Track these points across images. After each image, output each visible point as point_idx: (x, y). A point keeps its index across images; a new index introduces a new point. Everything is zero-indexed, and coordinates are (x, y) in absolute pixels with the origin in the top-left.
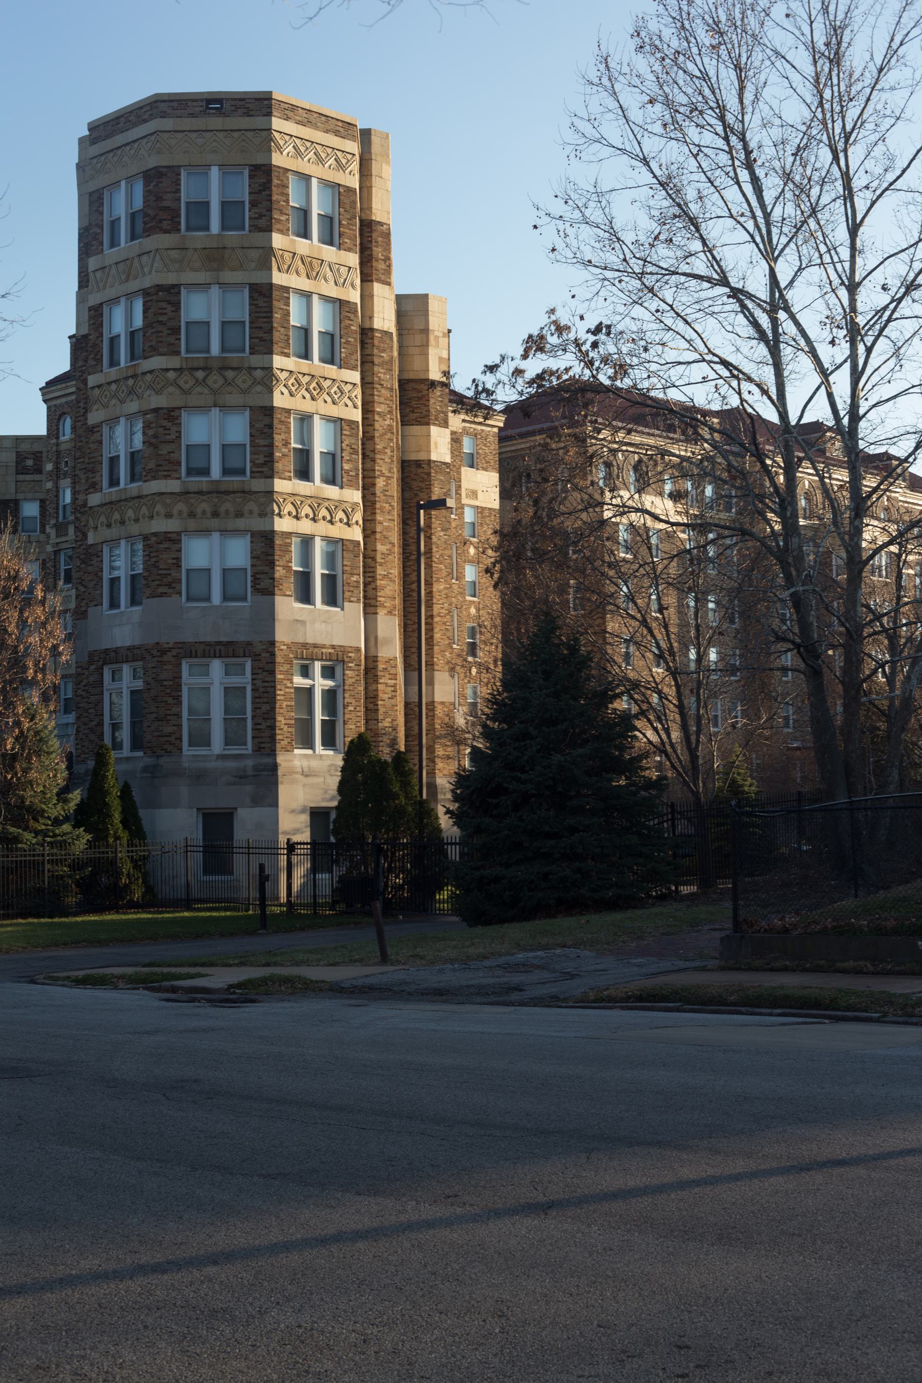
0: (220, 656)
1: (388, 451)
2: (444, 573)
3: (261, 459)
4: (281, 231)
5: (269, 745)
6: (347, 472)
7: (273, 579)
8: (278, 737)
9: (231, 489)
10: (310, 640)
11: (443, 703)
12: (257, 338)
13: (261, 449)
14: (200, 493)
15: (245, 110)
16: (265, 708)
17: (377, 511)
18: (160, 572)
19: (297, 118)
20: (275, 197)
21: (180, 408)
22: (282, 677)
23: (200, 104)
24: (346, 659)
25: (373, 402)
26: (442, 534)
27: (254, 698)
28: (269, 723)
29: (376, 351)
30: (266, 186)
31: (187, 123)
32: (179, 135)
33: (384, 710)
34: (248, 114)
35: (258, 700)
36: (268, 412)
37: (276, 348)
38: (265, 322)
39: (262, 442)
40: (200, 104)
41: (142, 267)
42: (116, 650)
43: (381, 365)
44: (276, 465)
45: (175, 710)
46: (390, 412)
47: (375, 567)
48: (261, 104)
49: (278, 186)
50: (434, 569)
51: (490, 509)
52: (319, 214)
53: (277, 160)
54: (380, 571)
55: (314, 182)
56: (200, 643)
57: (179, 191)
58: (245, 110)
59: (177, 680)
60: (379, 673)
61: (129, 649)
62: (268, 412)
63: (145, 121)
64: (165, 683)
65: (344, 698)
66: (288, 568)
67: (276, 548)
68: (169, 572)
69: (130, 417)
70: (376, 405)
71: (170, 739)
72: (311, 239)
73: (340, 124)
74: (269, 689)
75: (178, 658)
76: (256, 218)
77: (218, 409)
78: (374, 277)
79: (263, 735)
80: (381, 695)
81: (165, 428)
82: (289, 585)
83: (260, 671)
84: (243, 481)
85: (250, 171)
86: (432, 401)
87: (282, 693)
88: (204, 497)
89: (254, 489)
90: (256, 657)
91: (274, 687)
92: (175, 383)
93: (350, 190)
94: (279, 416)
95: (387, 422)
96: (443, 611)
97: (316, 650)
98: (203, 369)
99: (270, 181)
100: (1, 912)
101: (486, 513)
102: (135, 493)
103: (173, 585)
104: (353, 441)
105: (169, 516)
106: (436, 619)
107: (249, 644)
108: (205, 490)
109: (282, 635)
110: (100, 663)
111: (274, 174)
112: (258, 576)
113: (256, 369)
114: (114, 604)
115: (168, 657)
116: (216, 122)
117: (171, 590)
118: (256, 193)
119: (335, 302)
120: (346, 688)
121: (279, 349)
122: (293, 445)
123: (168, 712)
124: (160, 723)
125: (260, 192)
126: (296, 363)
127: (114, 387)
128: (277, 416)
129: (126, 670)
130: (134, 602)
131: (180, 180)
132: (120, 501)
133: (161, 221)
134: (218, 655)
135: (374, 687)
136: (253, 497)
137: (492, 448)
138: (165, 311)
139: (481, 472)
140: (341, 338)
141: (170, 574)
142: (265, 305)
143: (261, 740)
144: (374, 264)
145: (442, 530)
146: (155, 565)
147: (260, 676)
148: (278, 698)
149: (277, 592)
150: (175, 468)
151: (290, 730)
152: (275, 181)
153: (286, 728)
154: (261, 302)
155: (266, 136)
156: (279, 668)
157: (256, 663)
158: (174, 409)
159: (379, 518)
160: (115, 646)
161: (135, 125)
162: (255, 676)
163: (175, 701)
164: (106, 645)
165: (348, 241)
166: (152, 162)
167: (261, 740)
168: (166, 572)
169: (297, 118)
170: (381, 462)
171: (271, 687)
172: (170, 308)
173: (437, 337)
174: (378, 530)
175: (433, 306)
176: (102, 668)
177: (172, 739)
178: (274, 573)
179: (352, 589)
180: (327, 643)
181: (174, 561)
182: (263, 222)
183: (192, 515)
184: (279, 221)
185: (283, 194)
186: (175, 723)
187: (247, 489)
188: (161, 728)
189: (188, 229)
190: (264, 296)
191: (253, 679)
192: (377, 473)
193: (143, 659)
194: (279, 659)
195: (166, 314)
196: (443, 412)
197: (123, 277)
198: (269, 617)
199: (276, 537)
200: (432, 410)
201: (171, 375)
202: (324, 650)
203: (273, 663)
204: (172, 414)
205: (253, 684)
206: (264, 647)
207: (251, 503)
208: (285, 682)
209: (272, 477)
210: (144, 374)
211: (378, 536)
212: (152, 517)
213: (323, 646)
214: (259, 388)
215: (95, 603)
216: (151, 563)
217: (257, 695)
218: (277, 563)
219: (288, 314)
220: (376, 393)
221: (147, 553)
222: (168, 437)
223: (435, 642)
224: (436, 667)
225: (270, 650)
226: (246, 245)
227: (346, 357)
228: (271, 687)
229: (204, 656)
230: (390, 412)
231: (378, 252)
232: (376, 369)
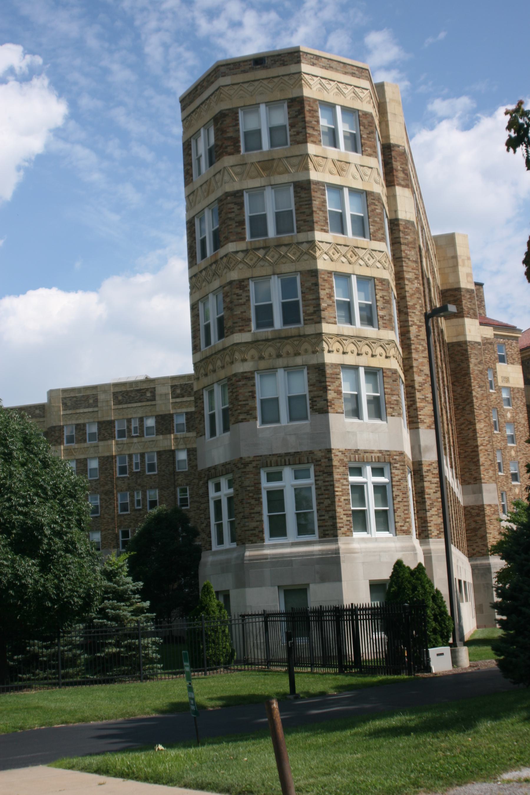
0: (289, 464)
1: (418, 306)
2: (483, 416)
3: (311, 309)
4: (314, 142)
5: (332, 532)
6: (382, 317)
7: (326, 400)
8: (339, 525)
9: (290, 335)
10: (361, 447)
11: (490, 505)
12: (301, 220)
13: (310, 302)
14: (267, 340)
15: (282, 62)
16: (327, 502)
17: (413, 351)
18: (240, 403)
19: (321, 64)
20: (308, 119)
21: (248, 279)
22: (339, 477)
23: (249, 63)
24: (392, 461)
25: (403, 271)
26: (479, 389)
27: (318, 495)
28: (331, 514)
29: (401, 235)
30: (301, 111)
31: (240, 78)
32: (236, 87)
33: (431, 502)
34: (284, 64)
35: (321, 497)
36: (314, 274)
37: (316, 227)
38: (307, 208)
39: (310, 297)
40: (249, 63)
41: (216, 183)
42: (215, 468)
43: (405, 244)
44: (323, 313)
45: (257, 509)
46: (417, 278)
47: (414, 393)
48: (294, 56)
49: (310, 111)
50: (476, 414)
51: (518, 388)
52: (344, 131)
53: (307, 92)
54: (418, 395)
55: (338, 109)
56: (273, 455)
57: (237, 124)
58: (282, 62)
59: (257, 486)
60: (424, 474)
61: (223, 465)
62: (314, 274)
63: (212, 83)
64: (248, 488)
65: (393, 492)
66: (339, 392)
67: (328, 376)
68: (246, 402)
69: (214, 292)
70: (405, 273)
71: (254, 532)
72: (339, 148)
73: (355, 68)
74: (329, 487)
75: (257, 469)
76: (294, 135)
77: (276, 276)
78: (396, 183)
79: (326, 524)
80: (427, 490)
81: (238, 295)
82: (343, 405)
83: (321, 473)
84: (299, 328)
85: (288, 103)
86: (464, 302)
87: (340, 489)
88: (270, 343)
89: (307, 333)
90: (317, 462)
91: (333, 485)
92: (243, 262)
93: (367, 115)
94: (323, 276)
95: (416, 285)
96: (485, 442)
97: (367, 454)
98: (264, 248)
99: (303, 108)
100: (1, 686)
101: (516, 391)
102: (220, 347)
103: (251, 412)
104: (385, 294)
105: (244, 360)
106: (480, 448)
107: (311, 452)
108: (270, 337)
109: (337, 443)
110: (206, 479)
111: (306, 103)
112: (315, 399)
113: (302, 243)
114: (213, 433)
115: (250, 468)
116: (261, 74)
117: (249, 416)
118: (293, 118)
119: (362, 193)
120: (394, 483)
121: (319, 227)
122: (336, 298)
123: (252, 511)
124: (246, 520)
125: (296, 116)
126: (334, 237)
127: (204, 273)
128: (321, 276)
129: (224, 482)
130: (226, 429)
131: (238, 117)
132: (212, 355)
133: (226, 147)
134: (287, 463)
135: (421, 485)
136: (307, 339)
137: (516, 350)
138: (233, 210)
139: (510, 365)
140: (369, 218)
141: (248, 404)
142: (306, 195)
143: (325, 528)
144: (395, 173)
145: (479, 387)
146: (237, 399)
147: (322, 478)
148: (337, 493)
149: (330, 409)
150: (247, 323)
151: (348, 519)
152: (307, 108)
153: (345, 518)
154: (303, 195)
155: (297, 78)
156: (335, 471)
157: (318, 467)
158: (243, 280)
159: (414, 355)
160: (214, 465)
161: (206, 88)
162: (317, 478)
163: (257, 502)
164: (209, 465)
165: (369, 149)
166: (216, 110)
167: (325, 528)
168: (244, 403)
169: (321, 64)
170: (413, 315)
171: (331, 485)
172: (236, 208)
173: (463, 260)
174: (414, 365)
175: (458, 241)
176: (207, 483)
177: (256, 532)
178: (327, 396)
179: (392, 406)
180: (375, 448)
181: (250, 394)
182: (300, 137)
183: (261, 358)
184: (312, 135)
185: (313, 117)
186: (258, 519)
187: (302, 333)
188: (247, 524)
189: (247, 150)
190: (305, 189)
191: (316, 480)
192: (410, 323)
193: (232, 471)
194: (335, 463)
195: (233, 212)
196: (472, 309)
197: (205, 194)
198: (325, 432)
199: (327, 368)
200: (465, 308)
201: (240, 256)
202: (373, 455)
203: (331, 466)
204: (243, 284)
205: (316, 484)
206: (323, 454)
207: (306, 344)
208: (341, 481)
209: (320, 322)
210: (222, 258)
211: (415, 369)
212: (232, 363)
213: (372, 452)
214: (306, 257)
215: (200, 434)
216: (234, 399)
217: (319, 493)
218: (329, 388)
219: (325, 201)
220: (404, 264)
221: (231, 390)
222: (240, 301)
223: (481, 463)
224: (483, 481)
225: (328, 456)
226: (289, 155)
227: (375, 232)
228: (331, 485)
229: (277, 465)
230: (417, 278)
231: (397, 165)
232: (403, 247)
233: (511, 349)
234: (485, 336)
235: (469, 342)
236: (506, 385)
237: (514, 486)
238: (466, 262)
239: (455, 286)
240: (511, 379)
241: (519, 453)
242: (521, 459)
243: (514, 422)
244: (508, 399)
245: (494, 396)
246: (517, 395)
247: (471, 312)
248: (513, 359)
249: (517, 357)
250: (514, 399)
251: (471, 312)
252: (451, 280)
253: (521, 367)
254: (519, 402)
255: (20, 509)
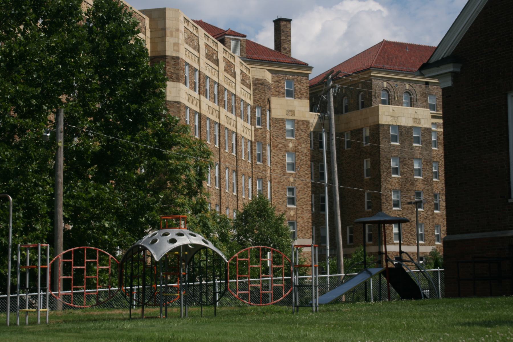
101: (300, 123)
137: (305, 86)
139: (297, 100)
173: (171, 32)
196: (175, 73)
233: (300, 85)
234: (256, 77)
236: (291, 118)
237: (289, 208)
238: (174, 33)
239: (162, 54)
240: (296, 112)
242: (299, 185)
243: (295, 152)
244: (292, 131)
245: (260, 131)
246: (302, 127)
247: (174, 76)
248: (301, 94)
249: (306, 91)
250: (297, 130)
251: (174, 76)
252: (159, 48)
253: (309, 101)
254: (303, 133)
255: (192, 153)
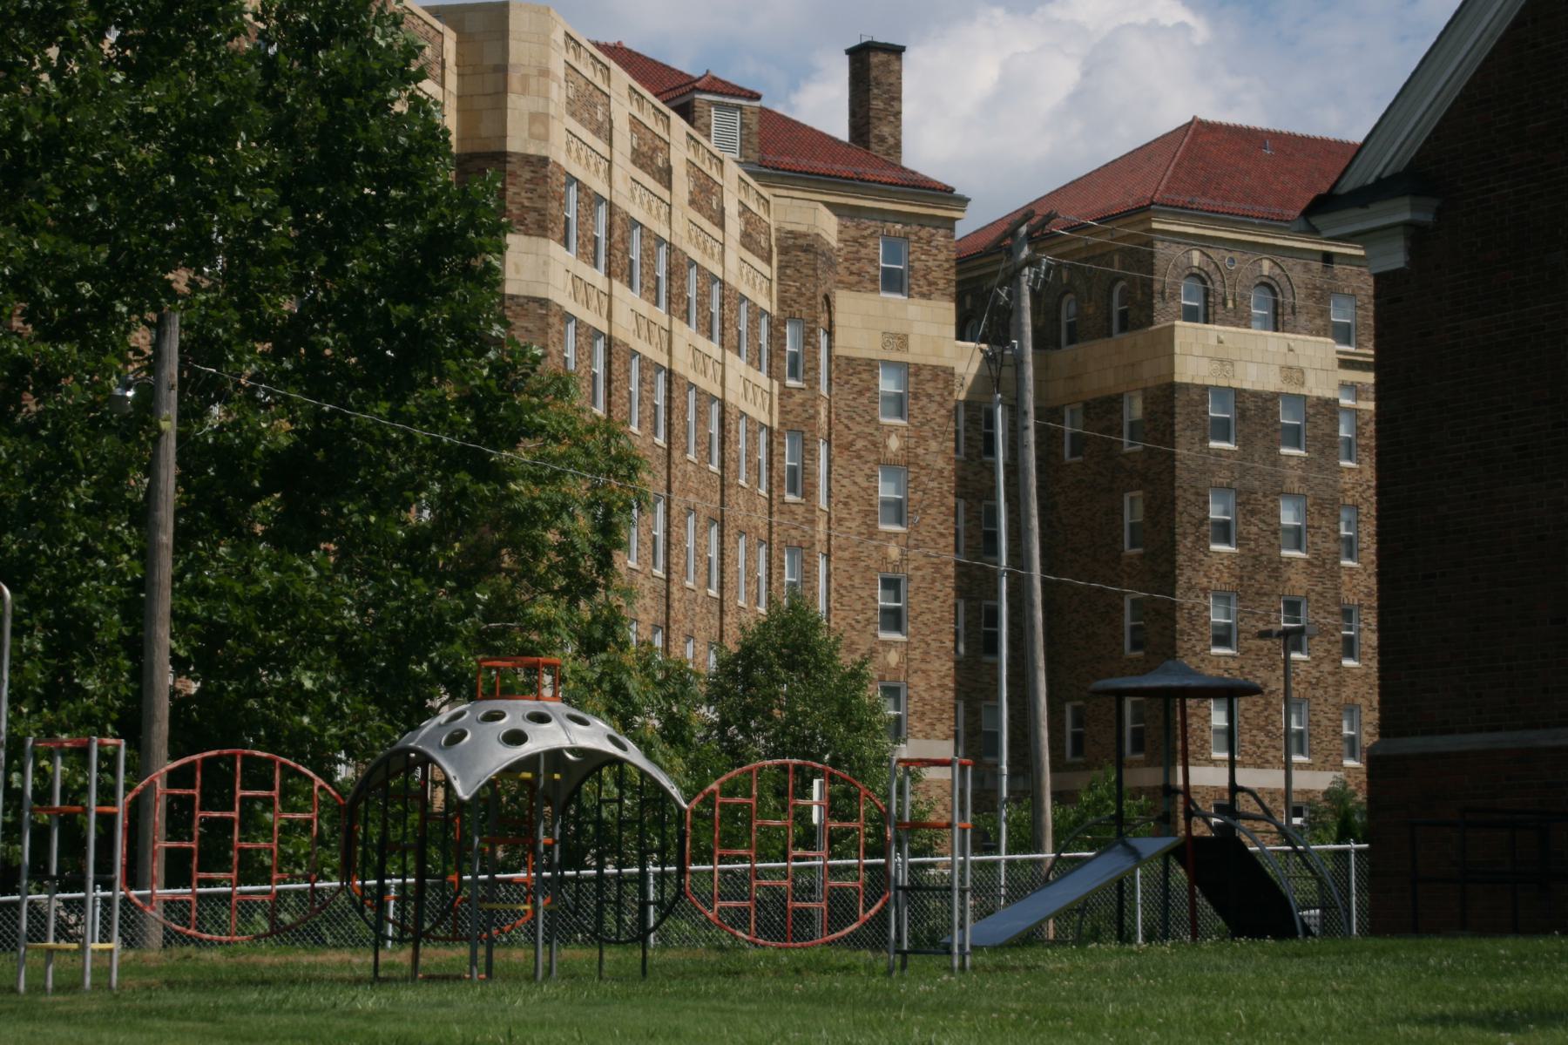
101: (926, 375)
137: (942, 257)
139: (917, 300)
173: (525, 79)
196: (535, 210)
233: (927, 253)
234: (789, 227)
235: (512, 297)
236: (896, 356)
238: (533, 82)
239: (494, 148)
240: (912, 341)
241: (913, 553)
242: (917, 569)
243: (908, 464)
245: (798, 398)
246: (929, 388)
247: (531, 218)
248: (930, 284)
249: (944, 275)
250: (916, 397)
251: (531, 218)
252: (486, 129)
253: (953, 306)
254: (934, 407)
